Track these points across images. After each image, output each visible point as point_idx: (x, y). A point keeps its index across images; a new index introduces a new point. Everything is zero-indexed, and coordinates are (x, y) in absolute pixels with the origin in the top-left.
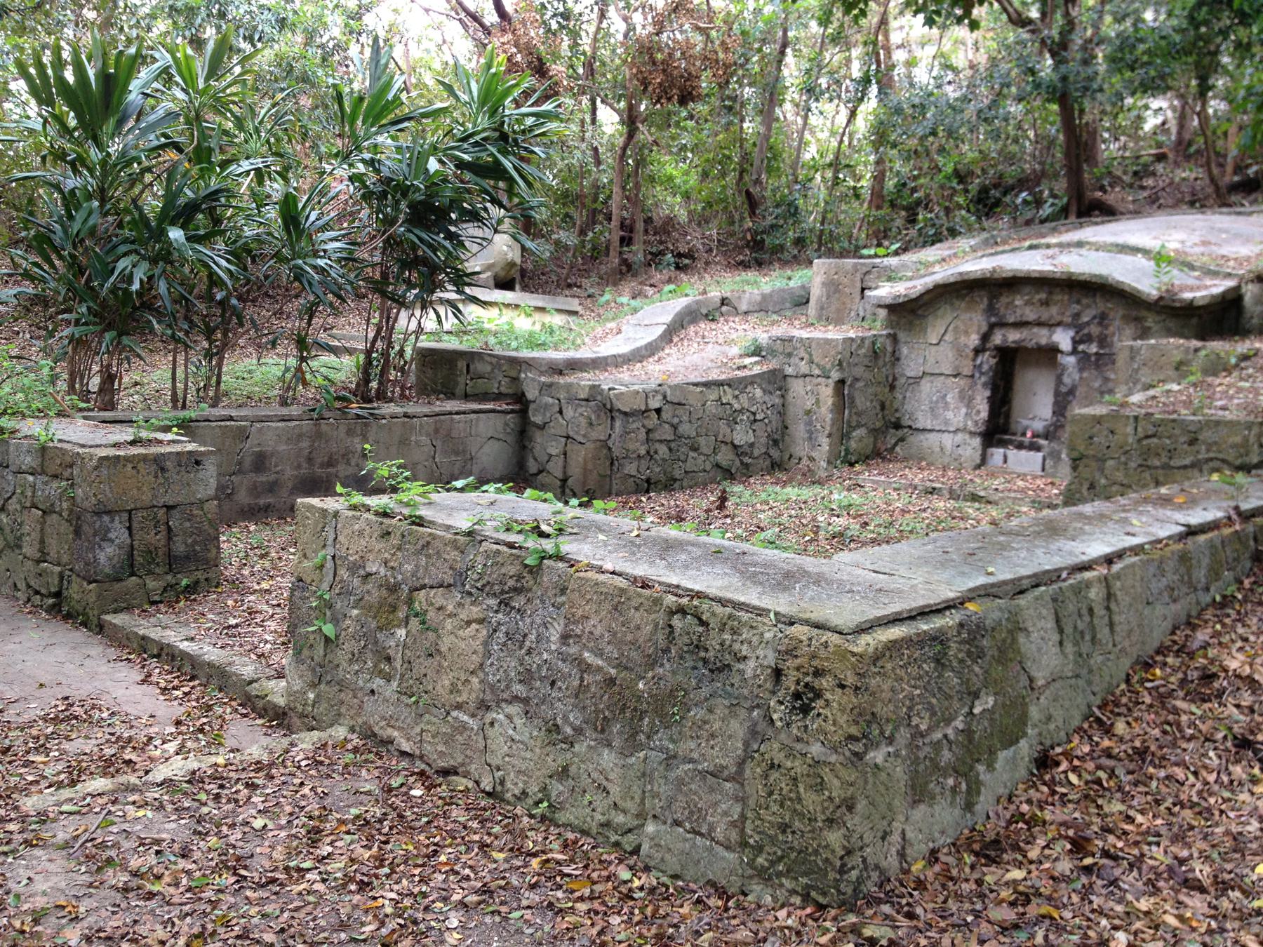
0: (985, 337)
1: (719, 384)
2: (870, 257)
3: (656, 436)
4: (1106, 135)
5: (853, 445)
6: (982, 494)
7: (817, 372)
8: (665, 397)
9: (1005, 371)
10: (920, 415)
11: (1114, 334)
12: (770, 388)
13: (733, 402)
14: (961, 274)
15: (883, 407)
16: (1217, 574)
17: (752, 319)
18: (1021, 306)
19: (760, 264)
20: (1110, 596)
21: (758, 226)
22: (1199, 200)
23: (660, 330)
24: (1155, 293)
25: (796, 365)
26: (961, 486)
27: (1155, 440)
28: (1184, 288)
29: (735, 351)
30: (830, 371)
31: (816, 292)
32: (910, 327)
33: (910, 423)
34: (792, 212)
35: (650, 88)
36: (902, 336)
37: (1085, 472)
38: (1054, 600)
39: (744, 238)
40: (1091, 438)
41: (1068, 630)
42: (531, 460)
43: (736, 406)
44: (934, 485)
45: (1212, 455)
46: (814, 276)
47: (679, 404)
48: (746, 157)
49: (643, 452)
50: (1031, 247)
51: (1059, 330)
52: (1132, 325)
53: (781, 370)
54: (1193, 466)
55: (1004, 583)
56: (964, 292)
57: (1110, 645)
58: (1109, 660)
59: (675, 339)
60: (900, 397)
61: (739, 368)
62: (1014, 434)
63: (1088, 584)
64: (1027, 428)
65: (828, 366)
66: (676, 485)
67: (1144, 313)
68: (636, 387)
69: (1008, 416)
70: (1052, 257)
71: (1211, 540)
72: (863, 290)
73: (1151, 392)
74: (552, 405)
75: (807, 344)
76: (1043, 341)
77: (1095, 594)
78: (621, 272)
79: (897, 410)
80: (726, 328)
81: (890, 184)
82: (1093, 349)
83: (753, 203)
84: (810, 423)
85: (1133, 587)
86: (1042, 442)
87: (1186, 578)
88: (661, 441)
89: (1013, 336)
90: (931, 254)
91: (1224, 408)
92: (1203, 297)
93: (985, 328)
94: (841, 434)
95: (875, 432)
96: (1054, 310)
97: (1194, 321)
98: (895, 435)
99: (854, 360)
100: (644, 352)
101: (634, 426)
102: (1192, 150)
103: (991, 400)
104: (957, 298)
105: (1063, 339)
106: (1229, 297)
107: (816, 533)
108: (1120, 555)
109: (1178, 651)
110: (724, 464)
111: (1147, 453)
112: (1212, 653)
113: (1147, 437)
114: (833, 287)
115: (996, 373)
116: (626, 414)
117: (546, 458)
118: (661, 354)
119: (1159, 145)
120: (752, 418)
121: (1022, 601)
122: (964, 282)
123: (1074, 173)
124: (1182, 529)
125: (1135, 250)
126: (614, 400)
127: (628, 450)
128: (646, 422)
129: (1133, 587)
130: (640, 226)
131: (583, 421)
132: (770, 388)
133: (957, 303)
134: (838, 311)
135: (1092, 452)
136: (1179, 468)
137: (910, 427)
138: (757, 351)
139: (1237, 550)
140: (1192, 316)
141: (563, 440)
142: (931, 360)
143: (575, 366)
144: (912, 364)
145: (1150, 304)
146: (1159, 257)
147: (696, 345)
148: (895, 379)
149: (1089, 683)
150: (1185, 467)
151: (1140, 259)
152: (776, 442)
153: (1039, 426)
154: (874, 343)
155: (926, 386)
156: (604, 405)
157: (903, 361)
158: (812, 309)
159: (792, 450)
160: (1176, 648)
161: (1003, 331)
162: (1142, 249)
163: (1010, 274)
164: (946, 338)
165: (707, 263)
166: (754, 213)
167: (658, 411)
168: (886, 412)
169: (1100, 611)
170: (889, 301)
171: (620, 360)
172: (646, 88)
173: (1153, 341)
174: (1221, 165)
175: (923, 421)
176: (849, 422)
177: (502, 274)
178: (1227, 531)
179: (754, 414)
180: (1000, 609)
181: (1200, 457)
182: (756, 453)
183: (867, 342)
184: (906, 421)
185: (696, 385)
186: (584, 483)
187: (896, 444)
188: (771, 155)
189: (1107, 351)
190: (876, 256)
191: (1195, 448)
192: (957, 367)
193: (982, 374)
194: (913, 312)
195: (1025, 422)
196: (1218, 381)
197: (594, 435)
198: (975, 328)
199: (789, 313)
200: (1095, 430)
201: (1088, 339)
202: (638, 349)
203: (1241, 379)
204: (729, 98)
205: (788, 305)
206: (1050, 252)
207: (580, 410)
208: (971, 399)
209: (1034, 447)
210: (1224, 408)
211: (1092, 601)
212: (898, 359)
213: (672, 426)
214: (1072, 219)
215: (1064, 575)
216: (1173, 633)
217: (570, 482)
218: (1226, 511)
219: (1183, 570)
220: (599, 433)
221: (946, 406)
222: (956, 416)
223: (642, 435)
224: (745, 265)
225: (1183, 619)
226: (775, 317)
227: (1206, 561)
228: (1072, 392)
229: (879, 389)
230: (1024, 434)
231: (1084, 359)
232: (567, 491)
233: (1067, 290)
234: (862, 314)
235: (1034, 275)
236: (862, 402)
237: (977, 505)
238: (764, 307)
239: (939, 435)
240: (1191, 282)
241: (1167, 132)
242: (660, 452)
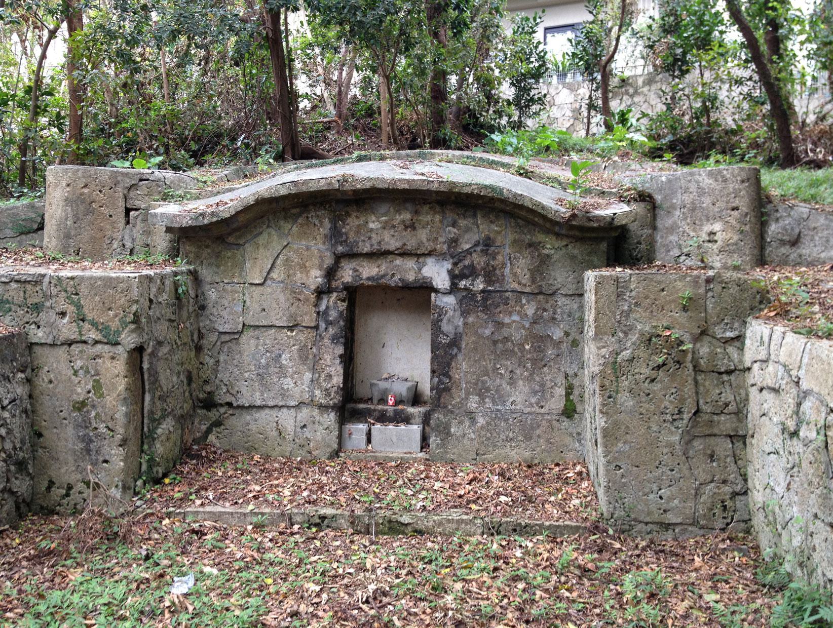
0: (331, 273)
5: (159, 448)
6: (406, 519)
7: (93, 335)
11: (504, 265)
18: (378, 230)
24: (564, 211)
30: (118, 333)
33: (229, 399)
36: (206, 273)
44: (323, 511)
51: (430, 261)
52: (526, 253)
53: (22, 336)
56: (294, 211)
60: (211, 362)
64: (385, 392)
65: (115, 325)
67: (540, 237)
72: (128, 211)
76: (411, 277)
79: (206, 382)
82: (479, 285)
84: (86, 424)
89: (369, 271)
93: (329, 261)
94: (142, 437)
96: (423, 234)
98: (206, 418)
99: (155, 312)
104: (285, 218)
105: (437, 273)
114: (82, 205)
133: (287, 226)
134: (93, 240)
137: (230, 405)
140: (602, 239)
142: (254, 307)
144: (224, 313)
145: (554, 223)
148: (201, 336)
152: (21, 465)
154: (176, 285)
155: (248, 343)
158: (50, 237)
159: (53, 473)
161: (354, 264)
163: (368, 185)
164: (274, 275)
168: (194, 385)
175: (249, 394)
176: (151, 412)
183: (167, 282)
184: (222, 397)
187: (209, 431)
192: (292, 316)
193: (329, 323)
194: (221, 239)
195: (383, 385)
201: (471, 272)
205: (8, 232)
208: (317, 359)
209: (402, 419)
212: (203, 308)
222: (298, 383)
228: (455, 342)
230: (383, 401)
231: (467, 301)
233: (438, 208)
234: (129, 245)
235: (401, 186)
239: (274, 412)
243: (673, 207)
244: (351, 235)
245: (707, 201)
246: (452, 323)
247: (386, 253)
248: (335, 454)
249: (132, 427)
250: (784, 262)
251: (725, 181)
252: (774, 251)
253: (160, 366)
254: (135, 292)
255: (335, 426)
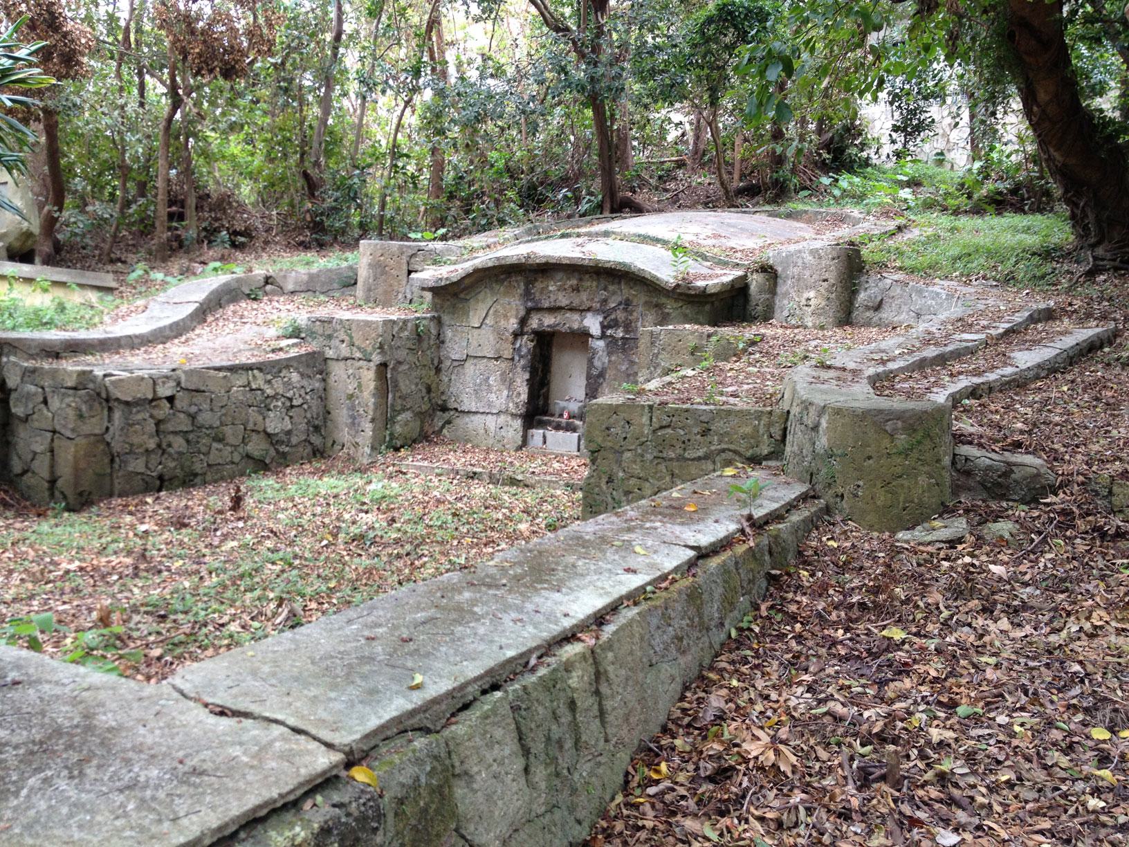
0: (523, 322)
1: (248, 368)
2: (415, 240)
3: (170, 427)
4: (635, 143)
5: (398, 429)
6: (520, 477)
7: (358, 355)
8: (179, 384)
9: (543, 354)
10: (464, 397)
12: (309, 372)
13: (266, 388)
14: (498, 259)
15: (429, 390)
16: (731, 604)
17: (298, 299)
18: (554, 291)
19: (321, 246)
20: (598, 675)
21: (318, 204)
22: (712, 201)
23: (191, 308)
24: (672, 282)
25: (337, 348)
26: (500, 471)
27: (669, 431)
28: (697, 277)
29: (272, 332)
30: (371, 354)
31: (363, 274)
32: (454, 310)
33: (456, 406)
34: (352, 195)
35: (190, 58)
36: (446, 319)
37: (604, 465)
38: (515, 709)
39: (304, 219)
40: (608, 429)
41: (538, 747)
42: (15, 458)
43: (269, 392)
44: (475, 469)
45: (724, 446)
46: (363, 257)
47: (197, 391)
48: (304, 142)
49: (152, 444)
50: (563, 236)
51: (589, 315)
53: (321, 353)
54: (706, 457)
55: (435, 701)
57: (602, 742)
58: (599, 764)
59: (210, 319)
61: (273, 351)
62: (552, 415)
63: (568, 667)
64: (563, 409)
65: (369, 349)
66: (198, 480)
67: (664, 300)
68: (140, 373)
69: (547, 397)
70: (581, 245)
71: (724, 563)
73: (668, 379)
74: (35, 394)
75: (347, 325)
76: (576, 326)
77: (577, 679)
78: (171, 249)
80: (268, 308)
81: (449, 176)
83: (312, 186)
84: (353, 408)
85: (631, 653)
86: (578, 423)
87: (697, 620)
88: (175, 433)
89: (549, 321)
90: (477, 240)
91: (734, 395)
92: (715, 285)
93: (522, 313)
94: (385, 419)
95: (421, 415)
96: (584, 296)
97: (708, 307)
100: (168, 333)
101: (139, 417)
102: (706, 158)
103: (530, 382)
105: (593, 324)
106: (737, 286)
107: (335, 536)
108: (614, 608)
109: (689, 725)
110: (256, 454)
111: (662, 444)
112: (729, 730)
113: (662, 427)
114: (379, 268)
115: (534, 356)
116: (127, 403)
117: (30, 457)
118: (191, 335)
119: (679, 153)
120: (288, 404)
121: (459, 729)
122: (501, 266)
123: (607, 172)
124: (692, 553)
125: (656, 241)
126: (111, 388)
127: (132, 445)
128: (155, 412)
129: (631, 653)
130: (192, 201)
131: (71, 413)
132: (309, 372)
133: (496, 287)
134: (386, 292)
135: (609, 444)
136: (693, 460)
137: (456, 409)
138: (296, 333)
139: (752, 570)
140: (706, 303)
141: (49, 435)
142: (474, 343)
143: (75, 348)
144: (456, 347)
146: (676, 247)
147: (231, 326)
148: (440, 362)
149: (572, 809)
150: (699, 459)
151: (659, 250)
152: (317, 429)
153: (574, 407)
154: (417, 326)
155: (470, 368)
156: (99, 394)
157: (448, 344)
158: (360, 290)
160: (687, 720)
161: (539, 316)
162: (666, 242)
163: (544, 260)
164: (487, 321)
165: (266, 243)
166: (313, 195)
167: (171, 399)
168: (433, 395)
169: (586, 702)
170: (431, 284)
171: (136, 341)
172: (185, 58)
173: (671, 327)
174: (730, 173)
175: (468, 403)
176: (392, 405)
177: (17, 244)
178: (740, 549)
179: (291, 400)
180: (418, 762)
181: (713, 448)
182: (294, 440)
184: (452, 405)
185: (219, 369)
186: (76, 485)
187: (443, 427)
188: (331, 143)
189: (632, 335)
190: (423, 239)
191: (709, 438)
192: (498, 351)
194: (455, 295)
195: (562, 404)
196: (729, 366)
197: (86, 428)
198: (514, 313)
199: (337, 295)
200: (612, 420)
201: (615, 324)
202: (161, 330)
203: (750, 364)
204: (284, 80)
205: (336, 286)
206: (580, 240)
207: (68, 400)
208: (512, 381)
209: (570, 428)
210: (734, 395)
211: (573, 690)
212: (443, 342)
213: (189, 415)
214: (607, 214)
215: (533, 661)
216: (682, 698)
217: (59, 483)
218: (739, 522)
219: (692, 611)
220: (94, 425)
221: (487, 391)
222: (499, 398)
223: (151, 426)
224: (305, 246)
225: (695, 672)
226: (322, 298)
227: (719, 591)
228: (602, 374)
229: (424, 372)
230: (561, 415)
231: (612, 343)
232: (57, 494)
234: (409, 296)
236: (406, 386)
237: (514, 490)
238: (311, 288)
239: (483, 417)
240: (705, 271)
241: (686, 143)
242: (175, 445)
243: (787, 277)
244: (537, 295)
245: (807, 273)
246: (602, 359)
247: (560, 308)
248: (520, 448)
249: (378, 413)
250: (868, 324)
251: (820, 258)
252: (859, 314)
253: (401, 378)
254: (380, 330)
255: (520, 429)
